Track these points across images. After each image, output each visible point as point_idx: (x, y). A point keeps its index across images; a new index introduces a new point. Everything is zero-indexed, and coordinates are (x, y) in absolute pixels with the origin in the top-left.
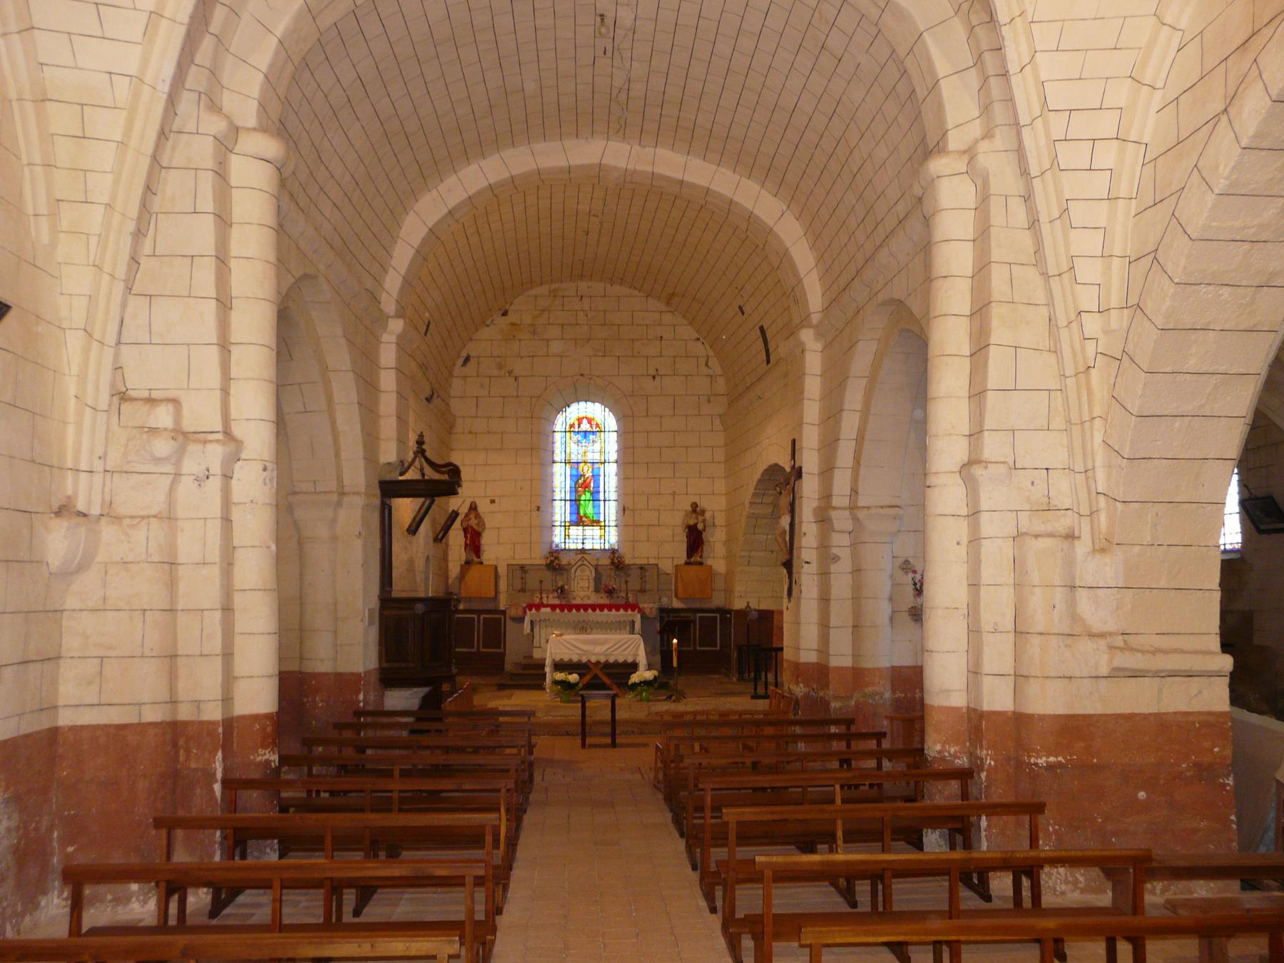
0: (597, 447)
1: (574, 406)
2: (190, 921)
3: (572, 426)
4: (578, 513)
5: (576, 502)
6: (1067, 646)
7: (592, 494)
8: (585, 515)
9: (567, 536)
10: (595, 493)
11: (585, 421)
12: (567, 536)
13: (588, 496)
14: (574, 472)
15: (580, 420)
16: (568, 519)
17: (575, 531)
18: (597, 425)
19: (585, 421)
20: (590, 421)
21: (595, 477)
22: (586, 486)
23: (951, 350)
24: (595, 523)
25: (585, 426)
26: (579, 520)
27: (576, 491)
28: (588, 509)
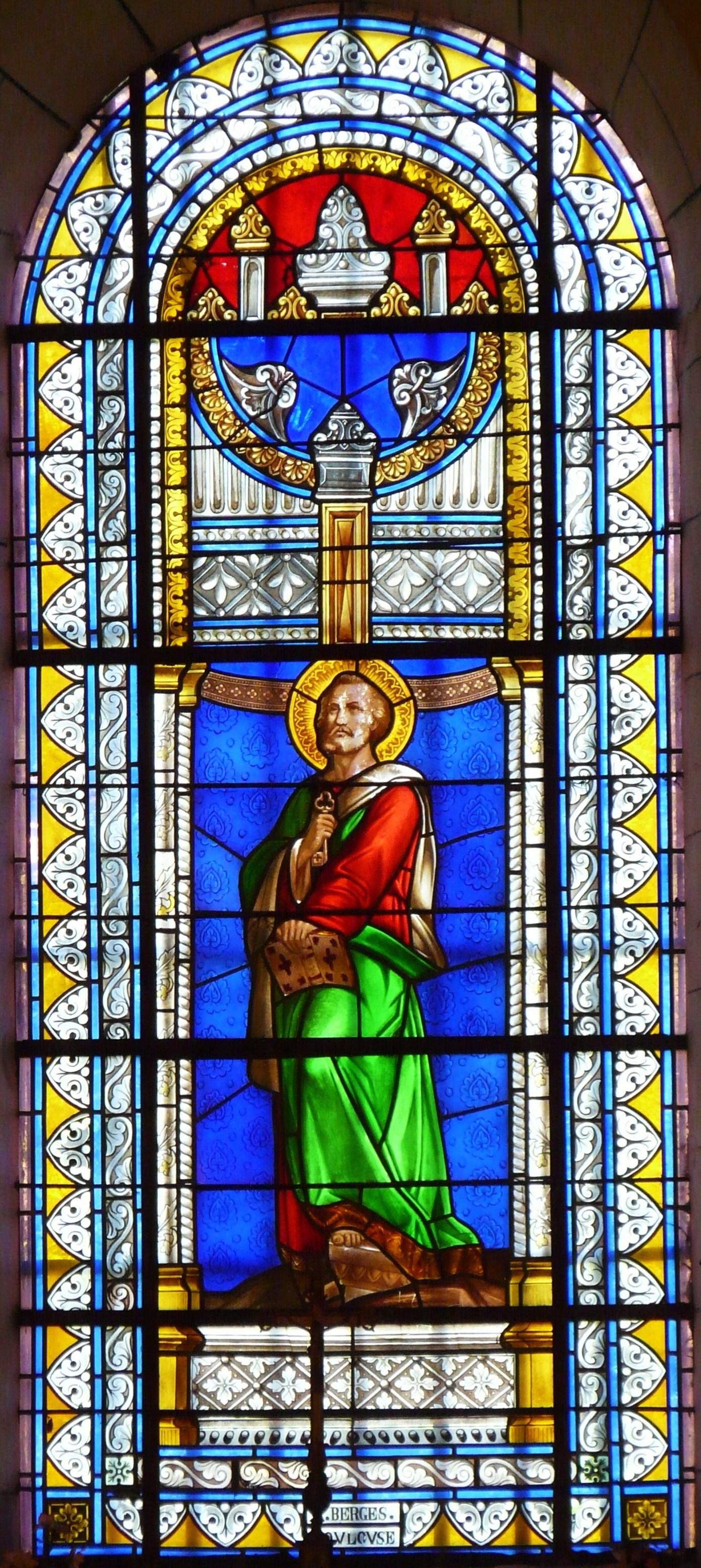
0: (473, 476)
1: (223, 77)
2: (317, 535)
3: (207, 265)
4: (283, 1178)
5: (255, 1070)
6: (224, 1364)
7: (425, 982)
8: (357, 1202)
9: (169, 1420)
10: (455, 972)
11: (340, 222)
12: (169, 1420)
13: (384, 998)
14: (237, 754)
15: (288, 208)
16: (175, 1244)
17: (241, 1370)
18: (471, 255)
19: (340, 222)
20: (393, 208)
21: (459, 803)
22: (356, 903)
23: (537, 931)
24: (461, 1277)
25: (343, 269)
26: (297, 1264)
27: (261, 955)
28: (390, 1136)
